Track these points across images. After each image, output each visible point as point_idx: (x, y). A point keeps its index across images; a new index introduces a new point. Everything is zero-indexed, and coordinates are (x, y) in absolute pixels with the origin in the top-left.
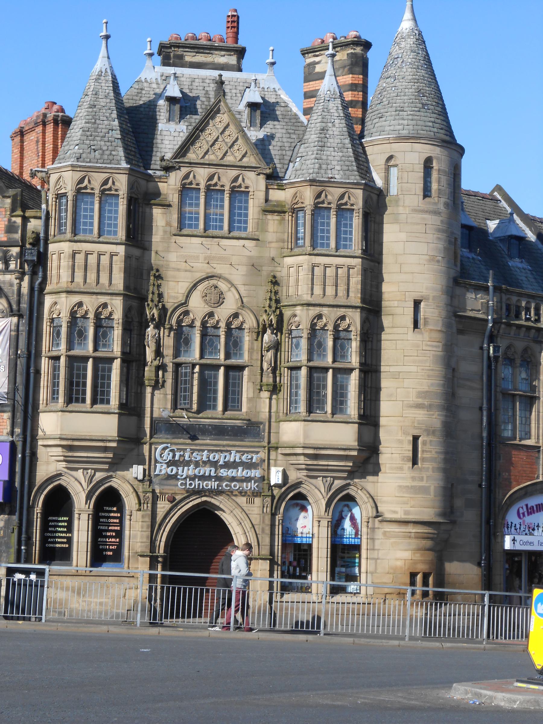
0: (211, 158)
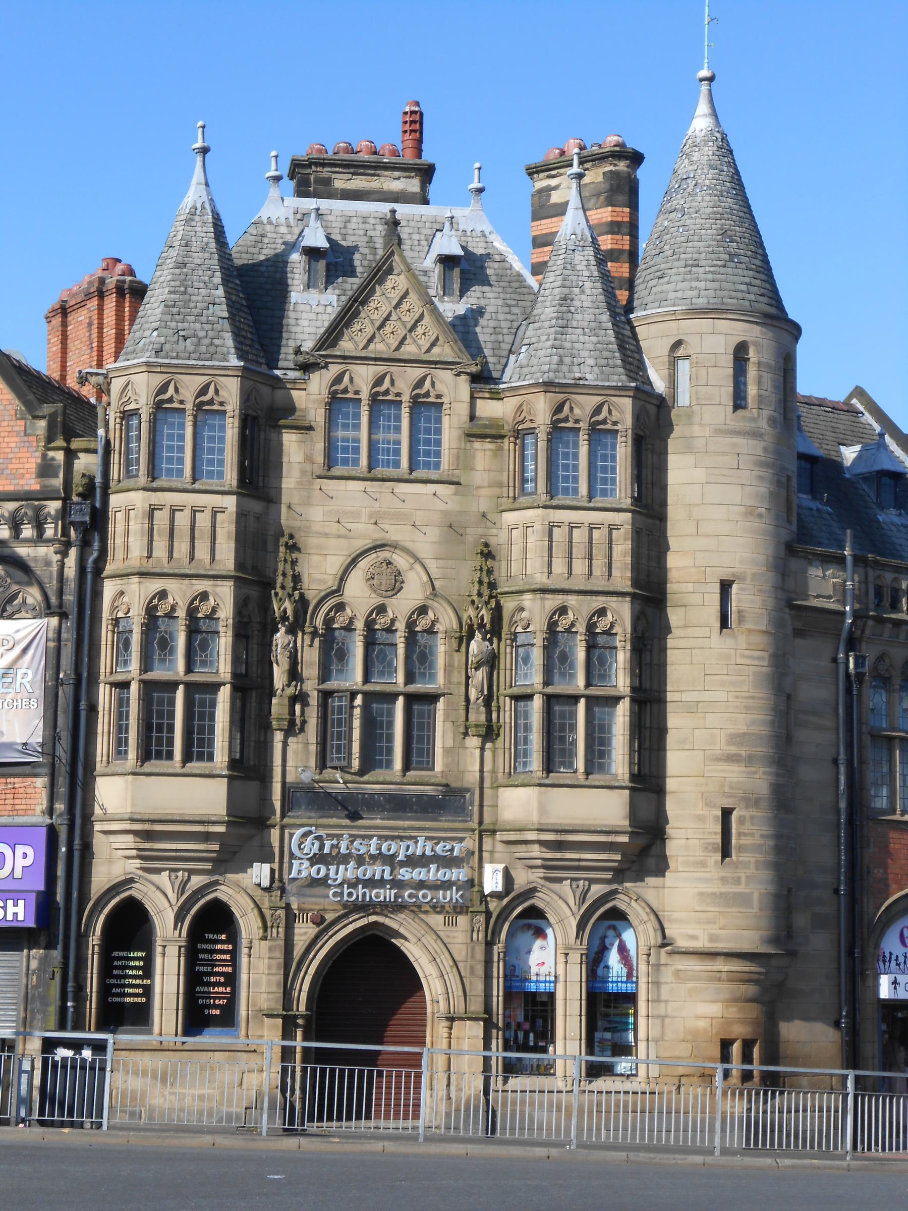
0: (378, 348)
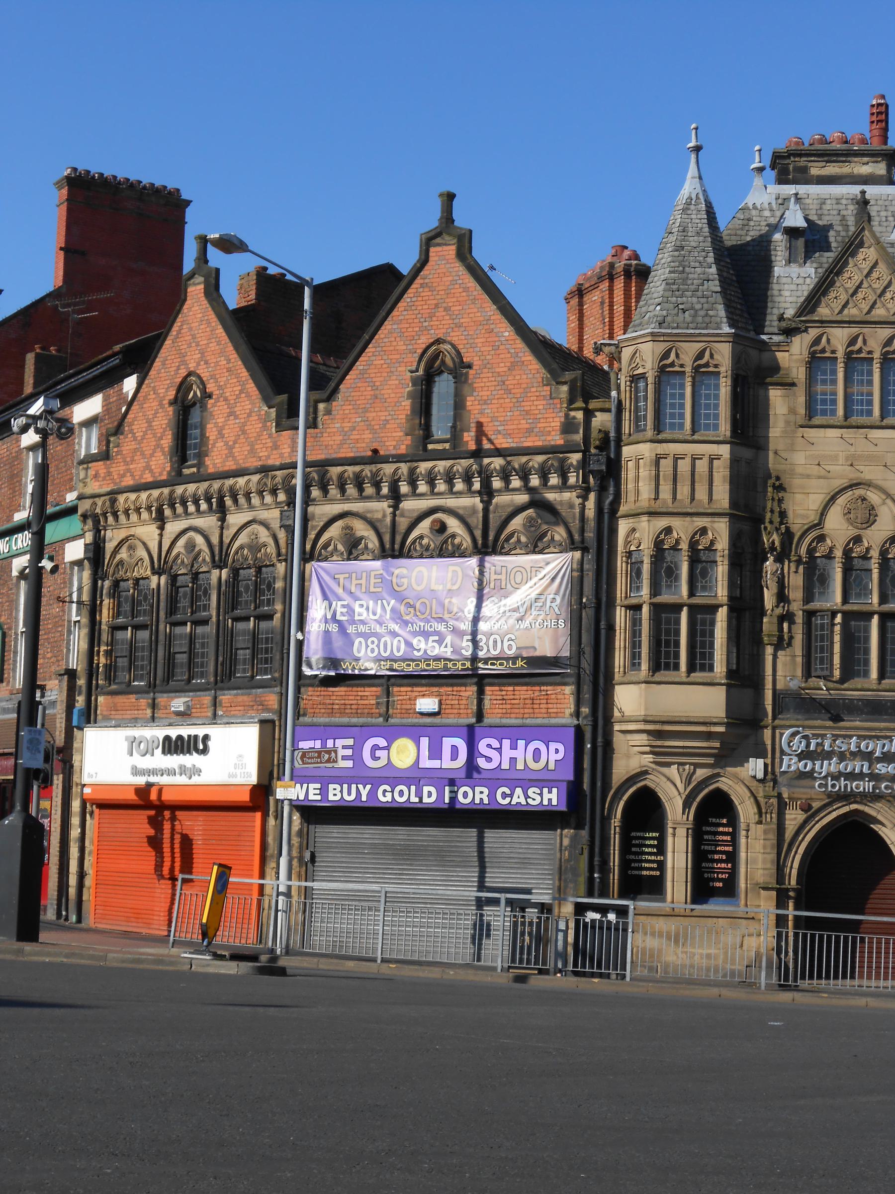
0: (852, 312)
